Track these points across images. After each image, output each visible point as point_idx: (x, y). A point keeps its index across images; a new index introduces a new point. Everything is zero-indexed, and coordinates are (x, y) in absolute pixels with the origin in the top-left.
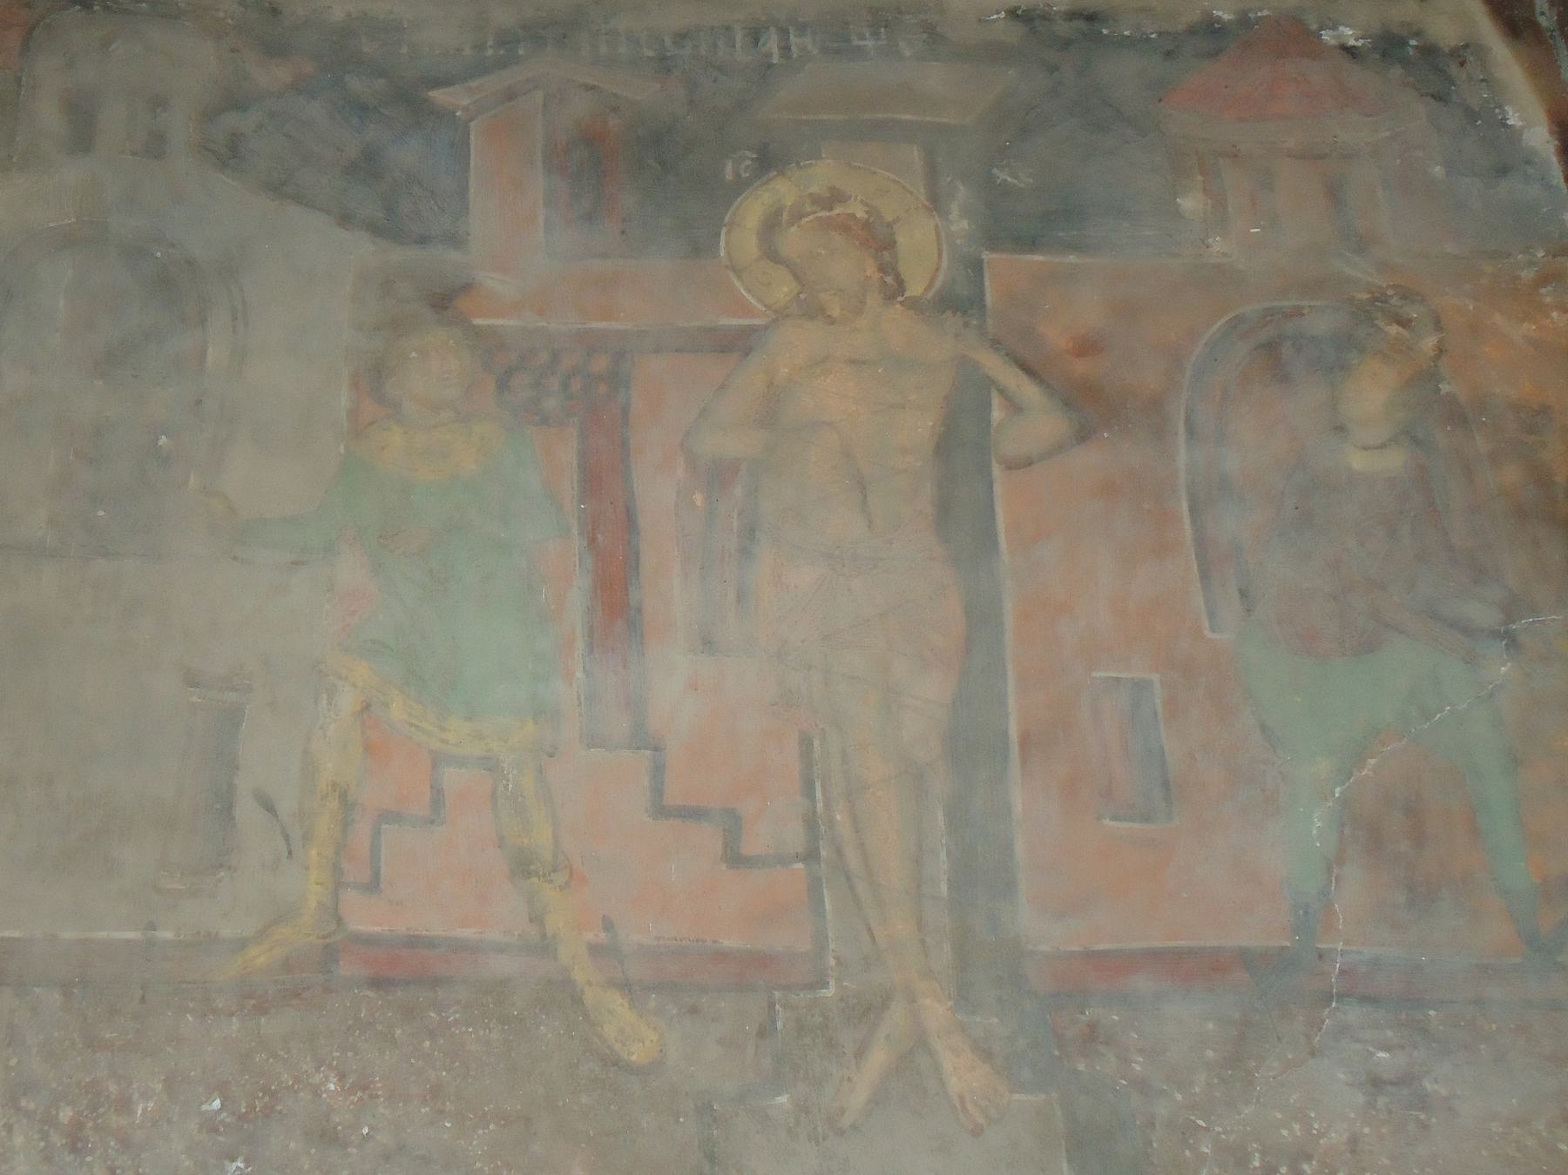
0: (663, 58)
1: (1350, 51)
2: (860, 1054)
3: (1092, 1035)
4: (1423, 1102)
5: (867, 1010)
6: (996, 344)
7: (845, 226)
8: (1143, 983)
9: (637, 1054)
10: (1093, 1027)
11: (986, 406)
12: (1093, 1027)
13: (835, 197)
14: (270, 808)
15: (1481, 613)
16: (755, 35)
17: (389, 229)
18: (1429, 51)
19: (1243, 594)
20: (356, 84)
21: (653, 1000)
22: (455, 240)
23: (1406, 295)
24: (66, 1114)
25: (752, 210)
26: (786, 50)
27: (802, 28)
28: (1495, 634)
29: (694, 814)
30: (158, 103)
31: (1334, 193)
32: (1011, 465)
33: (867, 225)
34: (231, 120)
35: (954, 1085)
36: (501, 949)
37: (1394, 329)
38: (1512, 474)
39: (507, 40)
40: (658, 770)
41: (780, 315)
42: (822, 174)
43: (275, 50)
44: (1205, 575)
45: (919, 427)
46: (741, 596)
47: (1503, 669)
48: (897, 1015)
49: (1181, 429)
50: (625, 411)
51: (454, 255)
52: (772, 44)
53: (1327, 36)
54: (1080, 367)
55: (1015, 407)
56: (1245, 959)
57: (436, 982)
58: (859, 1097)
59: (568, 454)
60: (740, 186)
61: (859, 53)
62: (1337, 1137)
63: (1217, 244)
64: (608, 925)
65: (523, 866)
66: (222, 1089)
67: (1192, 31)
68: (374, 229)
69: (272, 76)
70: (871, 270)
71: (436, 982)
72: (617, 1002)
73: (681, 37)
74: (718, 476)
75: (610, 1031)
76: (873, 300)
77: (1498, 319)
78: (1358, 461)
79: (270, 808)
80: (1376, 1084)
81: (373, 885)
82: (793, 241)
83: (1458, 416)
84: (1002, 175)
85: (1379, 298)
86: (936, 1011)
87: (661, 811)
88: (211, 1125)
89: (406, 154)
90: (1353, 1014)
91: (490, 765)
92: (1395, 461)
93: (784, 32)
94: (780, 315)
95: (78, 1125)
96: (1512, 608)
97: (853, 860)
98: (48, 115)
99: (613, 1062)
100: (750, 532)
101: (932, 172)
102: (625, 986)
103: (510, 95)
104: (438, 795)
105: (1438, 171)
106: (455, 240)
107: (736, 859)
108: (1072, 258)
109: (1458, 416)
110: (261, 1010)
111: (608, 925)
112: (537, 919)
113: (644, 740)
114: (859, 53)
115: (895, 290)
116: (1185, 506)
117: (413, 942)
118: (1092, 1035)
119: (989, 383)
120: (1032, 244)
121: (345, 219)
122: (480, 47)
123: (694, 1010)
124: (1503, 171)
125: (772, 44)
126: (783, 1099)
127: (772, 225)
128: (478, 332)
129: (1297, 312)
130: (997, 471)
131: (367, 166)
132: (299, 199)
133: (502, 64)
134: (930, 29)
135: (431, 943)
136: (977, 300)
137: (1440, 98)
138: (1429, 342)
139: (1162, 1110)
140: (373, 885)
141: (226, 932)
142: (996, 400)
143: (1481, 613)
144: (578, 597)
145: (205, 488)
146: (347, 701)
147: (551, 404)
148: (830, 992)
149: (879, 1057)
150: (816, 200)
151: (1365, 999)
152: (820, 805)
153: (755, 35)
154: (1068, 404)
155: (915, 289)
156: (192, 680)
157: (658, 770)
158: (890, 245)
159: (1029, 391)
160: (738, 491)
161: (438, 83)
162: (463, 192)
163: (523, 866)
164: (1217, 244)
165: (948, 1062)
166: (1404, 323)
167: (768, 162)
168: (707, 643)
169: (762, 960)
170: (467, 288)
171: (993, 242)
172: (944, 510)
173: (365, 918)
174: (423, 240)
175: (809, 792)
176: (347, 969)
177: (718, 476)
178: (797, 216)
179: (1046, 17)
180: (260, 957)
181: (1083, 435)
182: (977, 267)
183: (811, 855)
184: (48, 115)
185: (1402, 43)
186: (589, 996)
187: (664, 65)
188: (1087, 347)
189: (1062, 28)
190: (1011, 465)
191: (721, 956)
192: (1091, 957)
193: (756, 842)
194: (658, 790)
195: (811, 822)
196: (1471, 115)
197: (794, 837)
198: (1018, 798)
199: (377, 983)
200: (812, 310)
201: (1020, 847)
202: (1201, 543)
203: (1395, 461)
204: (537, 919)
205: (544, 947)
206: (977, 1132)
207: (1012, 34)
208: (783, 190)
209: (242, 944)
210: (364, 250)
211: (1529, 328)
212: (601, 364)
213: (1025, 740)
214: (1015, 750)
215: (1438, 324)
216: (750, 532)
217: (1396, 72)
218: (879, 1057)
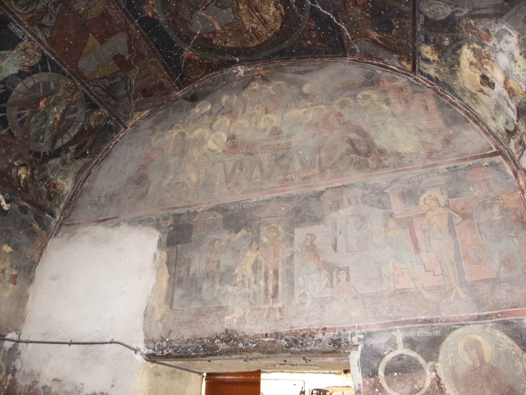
0: (408, 182)
1: (487, 166)
2: (452, 295)
3: (476, 290)
4: (514, 292)
5: (452, 290)
6: (452, 210)
7: (433, 199)
8: (481, 283)
9: (428, 298)
10: (476, 289)
11: (452, 218)
12: (476, 289)
13: (431, 195)
14: (386, 276)
15: (513, 234)
16: (418, 177)
17: (384, 208)
18: (496, 164)
19: (485, 236)
20: (376, 191)
21: (429, 292)
22: (391, 208)
23: (498, 196)
24: (373, 310)
25: (422, 198)
26: (422, 178)
27: (423, 175)
28: (515, 237)
29: (430, 271)
30: (357, 198)
31: (488, 185)
32: (457, 225)
33: (435, 198)
34: (364, 198)
35: (462, 297)
36: (412, 288)
37: (497, 201)
38: (514, 217)
39: (391, 183)
40: (425, 267)
41: (428, 211)
42: (429, 193)
43: (367, 189)
44: (480, 235)
45: (446, 222)
46: (430, 245)
47: (516, 241)
48: (455, 291)
49: (475, 217)
50: (413, 225)
51: (391, 210)
52: (420, 177)
53: (483, 164)
54: (462, 211)
55: (456, 218)
56: (492, 279)
57: (407, 293)
58: (452, 300)
59: (408, 232)
60: (420, 196)
61: (430, 177)
62: (504, 298)
63: (475, 194)
64: (423, 285)
65: (413, 279)
66: (388, 306)
67: (468, 166)
68: (382, 208)
69: (368, 192)
70: (437, 204)
71: (407, 293)
72: (425, 293)
73: (410, 179)
74: (425, 231)
75: (425, 296)
76: (437, 207)
77: (510, 198)
78: (496, 218)
79: (386, 276)
80: (508, 291)
81: (398, 283)
82: (427, 201)
83: (507, 211)
84: (449, 189)
85: (495, 198)
86: (459, 289)
87: (426, 271)
88: (387, 310)
89: (383, 199)
90: (504, 284)
91: (407, 268)
92: (500, 217)
93: (421, 176)
94: (428, 211)
95: (375, 311)
96: (516, 233)
97: (447, 274)
98: (346, 201)
99: (426, 299)
100: (429, 237)
101: (441, 190)
102: (426, 291)
103: (393, 189)
104: (403, 273)
105: (499, 180)
106: (391, 208)
107: (435, 275)
108: (459, 198)
109: (507, 211)
110: (390, 298)
111: (423, 285)
112: (415, 285)
113: (423, 263)
114: (430, 177)
115: (440, 206)
116: (477, 226)
117: (403, 289)
118: (476, 290)
119: (452, 215)
120: (454, 197)
121: (379, 208)
122: (388, 184)
123: (433, 293)
124: (507, 178)
125: (420, 177)
126: (444, 301)
127: (424, 200)
128: (396, 219)
129: (486, 201)
130: (455, 226)
131: (380, 201)
132: (373, 206)
133: (391, 186)
134: (437, 172)
135: (405, 289)
136: (449, 205)
137: (498, 170)
138: (502, 202)
139: (485, 297)
140: (398, 283)
141: (384, 290)
142: (453, 217)
143: (513, 234)
144: (412, 248)
145: (359, 237)
146: (391, 263)
147: (405, 226)
148: (447, 289)
149: (454, 295)
150: (429, 196)
151: (506, 282)
152: (422, 81)
153: (418, 177)
154: (462, 216)
155: (442, 205)
156: (375, 263)
157: (425, 267)
158: (438, 200)
159: (457, 215)
160: (427, 233)
161: (385, 189)
162: (390, 202)
163: (413, 279)
164: (475, 194)
165: (461, 294)
166: (498, 200)
167: (423, 192)
168: (427, 251)
169: (440, 286)
170: (393, 214)
171: (450, 198)
172: (450, 231)
173: (398, 287)
174: (387, 209)
175: (441, 266)
176: (397, 293)
177: (425, 231)
178: (427, 198)
179: (450, 168)
180: (388, 292)
181: (464, 220)
182: (448, 201)
183: (443, 274)
184: (346, 201)
185: (493, 164)
186: (422, 292)
187: (409, 183)
188: (463, 209)
189: (452, 169)
190: (457, 225)
191: (435, 286)
192: (474, 281)
193: (436, 274)
194: (425, 269)
195: (442, 270)
196: (503, 172)
197: (440, 272)
198: (464, 264)
199: (401, 294)
200: (431, 210)
201: (465, 270)
202: (479, 231)
203: (500, 217)
204: (415, 285)
205: (417, 288)
206: (465, 302)
207: (447, 171)
208: (425, 195)
209: (386, 291)
210: (382, 211)
211: (513, 198)
212: (409, 220)
213: (464, 258)
214: (463, 259)
215: (502, 199)
216: (429, 237)
217: (492, 168)
218: (454, 295)
